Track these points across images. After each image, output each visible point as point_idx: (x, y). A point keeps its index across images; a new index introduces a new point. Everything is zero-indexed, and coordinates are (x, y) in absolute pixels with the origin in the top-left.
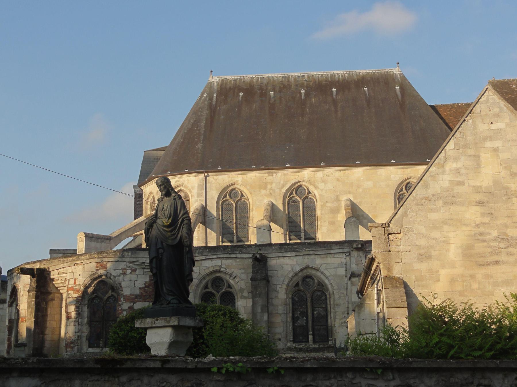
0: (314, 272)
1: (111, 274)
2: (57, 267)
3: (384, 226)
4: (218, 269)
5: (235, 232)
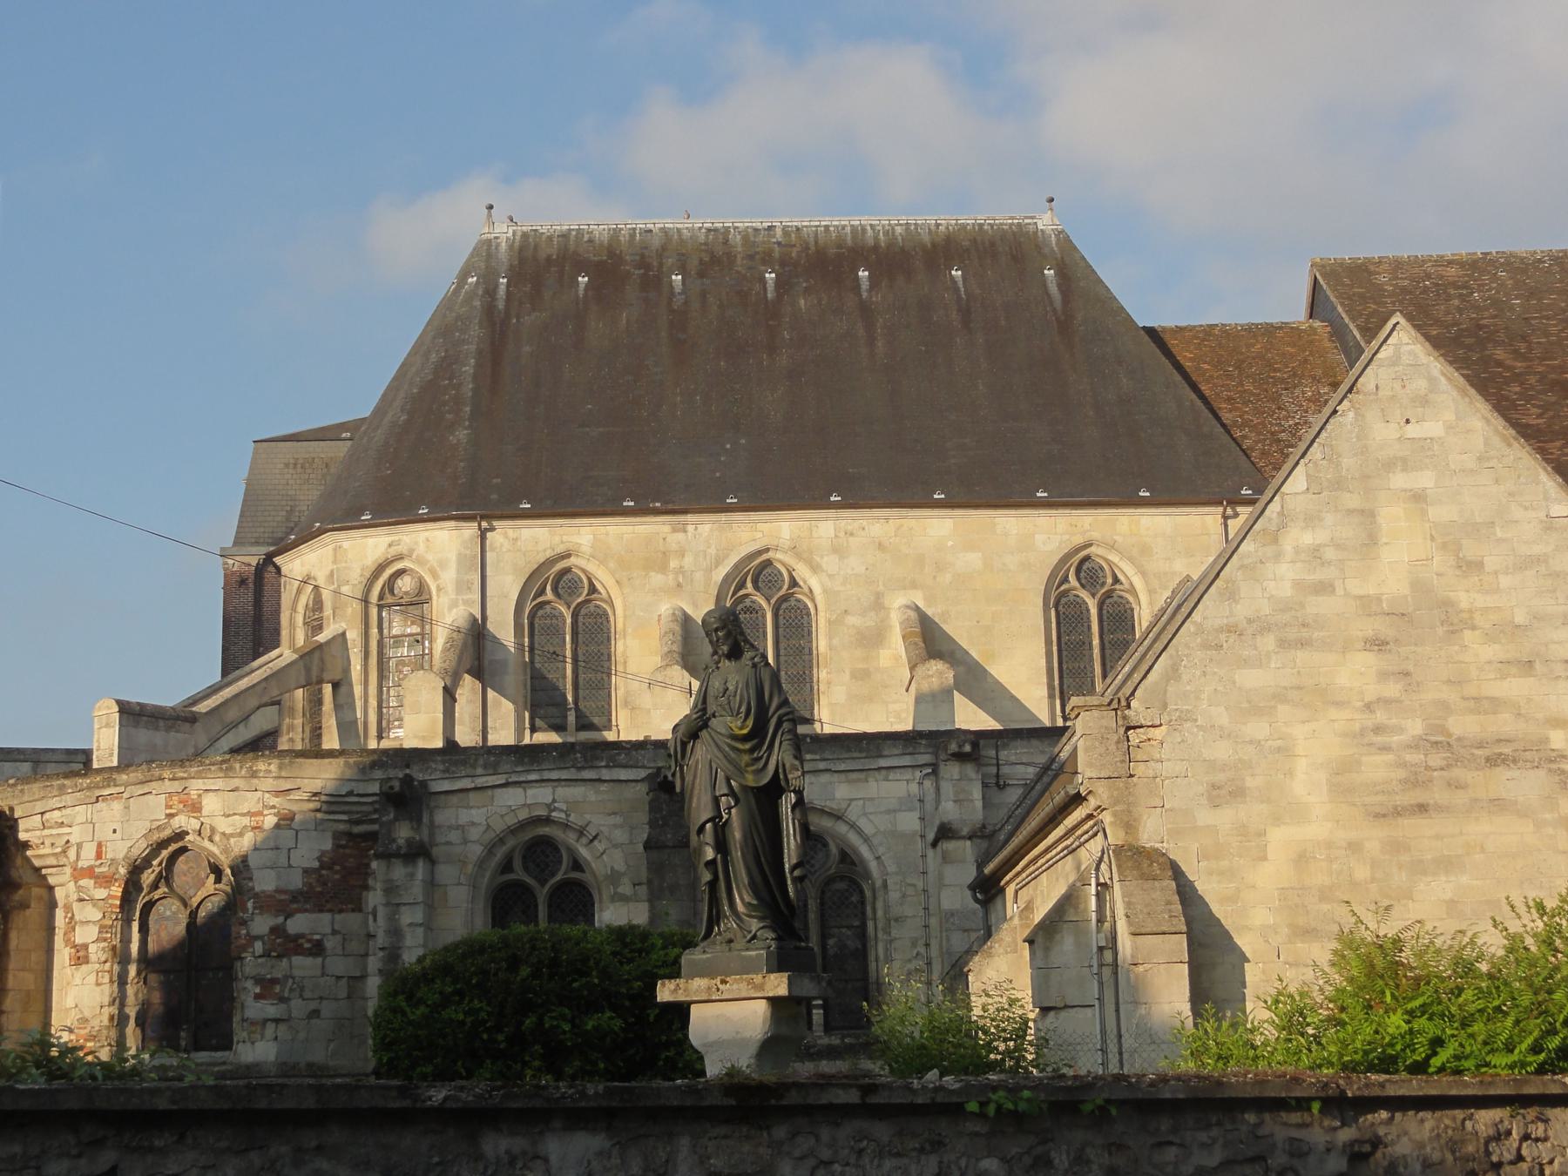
1: (213, 830)
2: (39, 807)
3: (1115, 705)
4: (543, 812)
5: (570, 698)
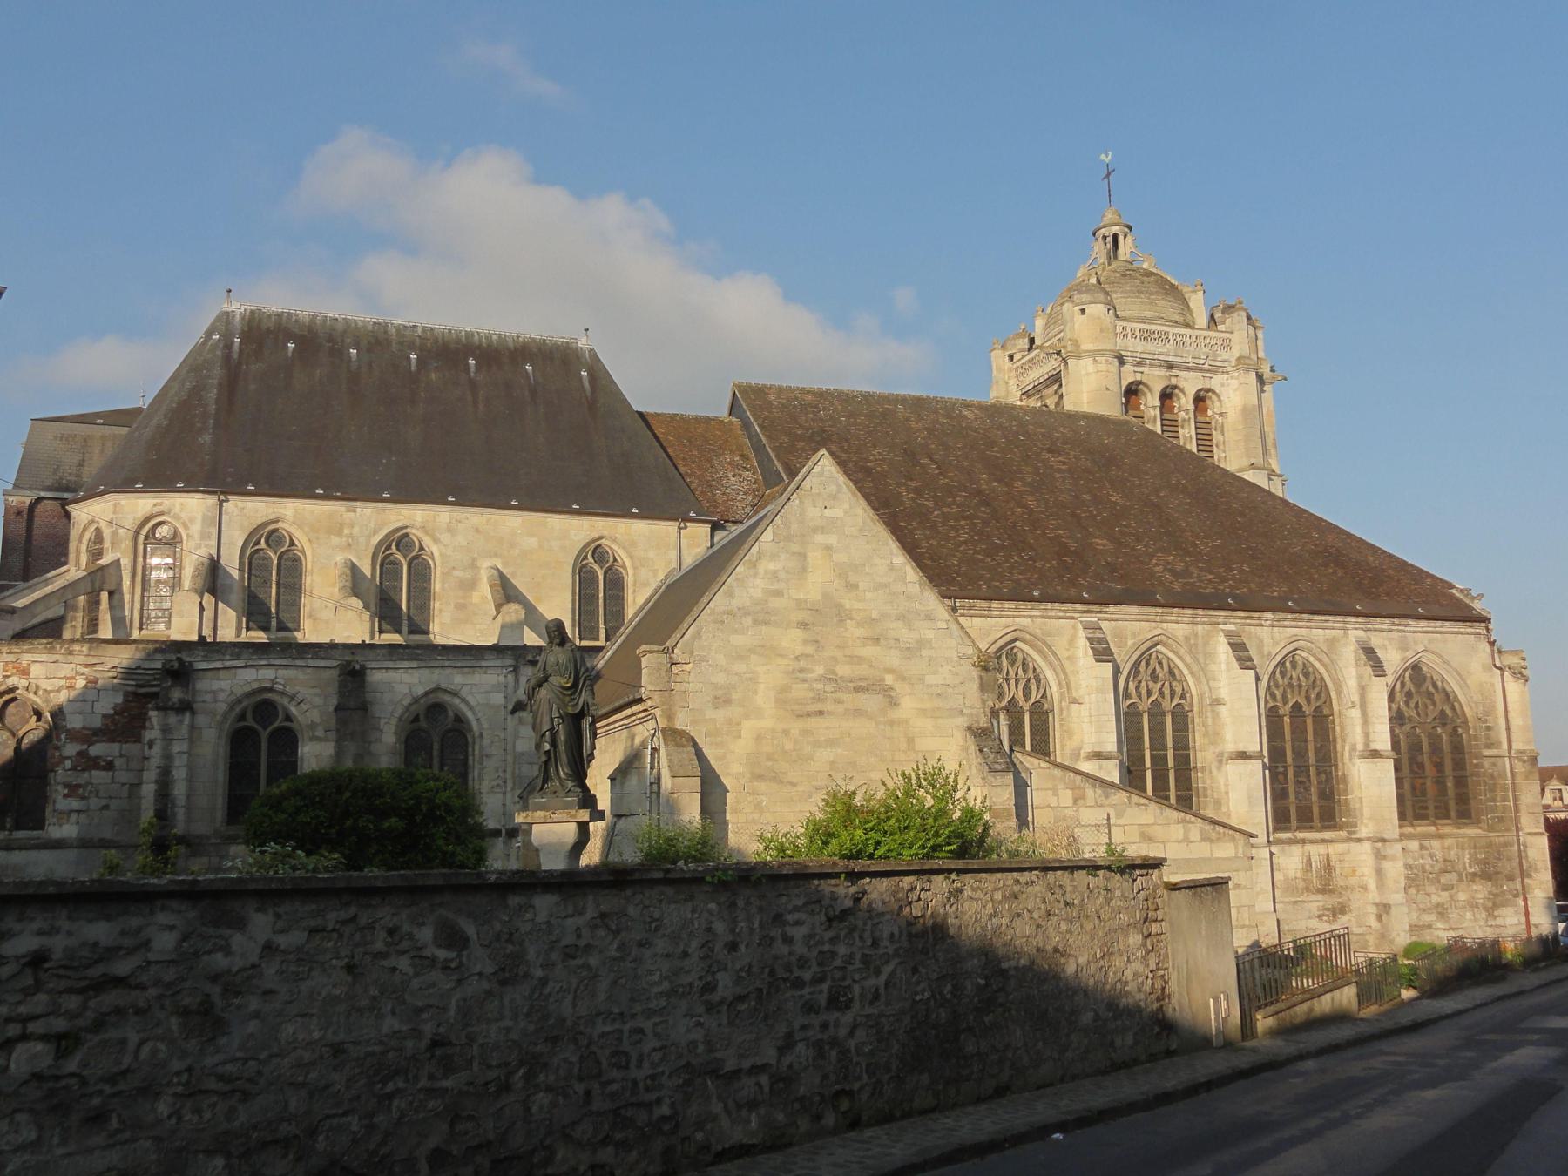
0: (447, 698)
1: (37, 687)
4: (268, 685)
